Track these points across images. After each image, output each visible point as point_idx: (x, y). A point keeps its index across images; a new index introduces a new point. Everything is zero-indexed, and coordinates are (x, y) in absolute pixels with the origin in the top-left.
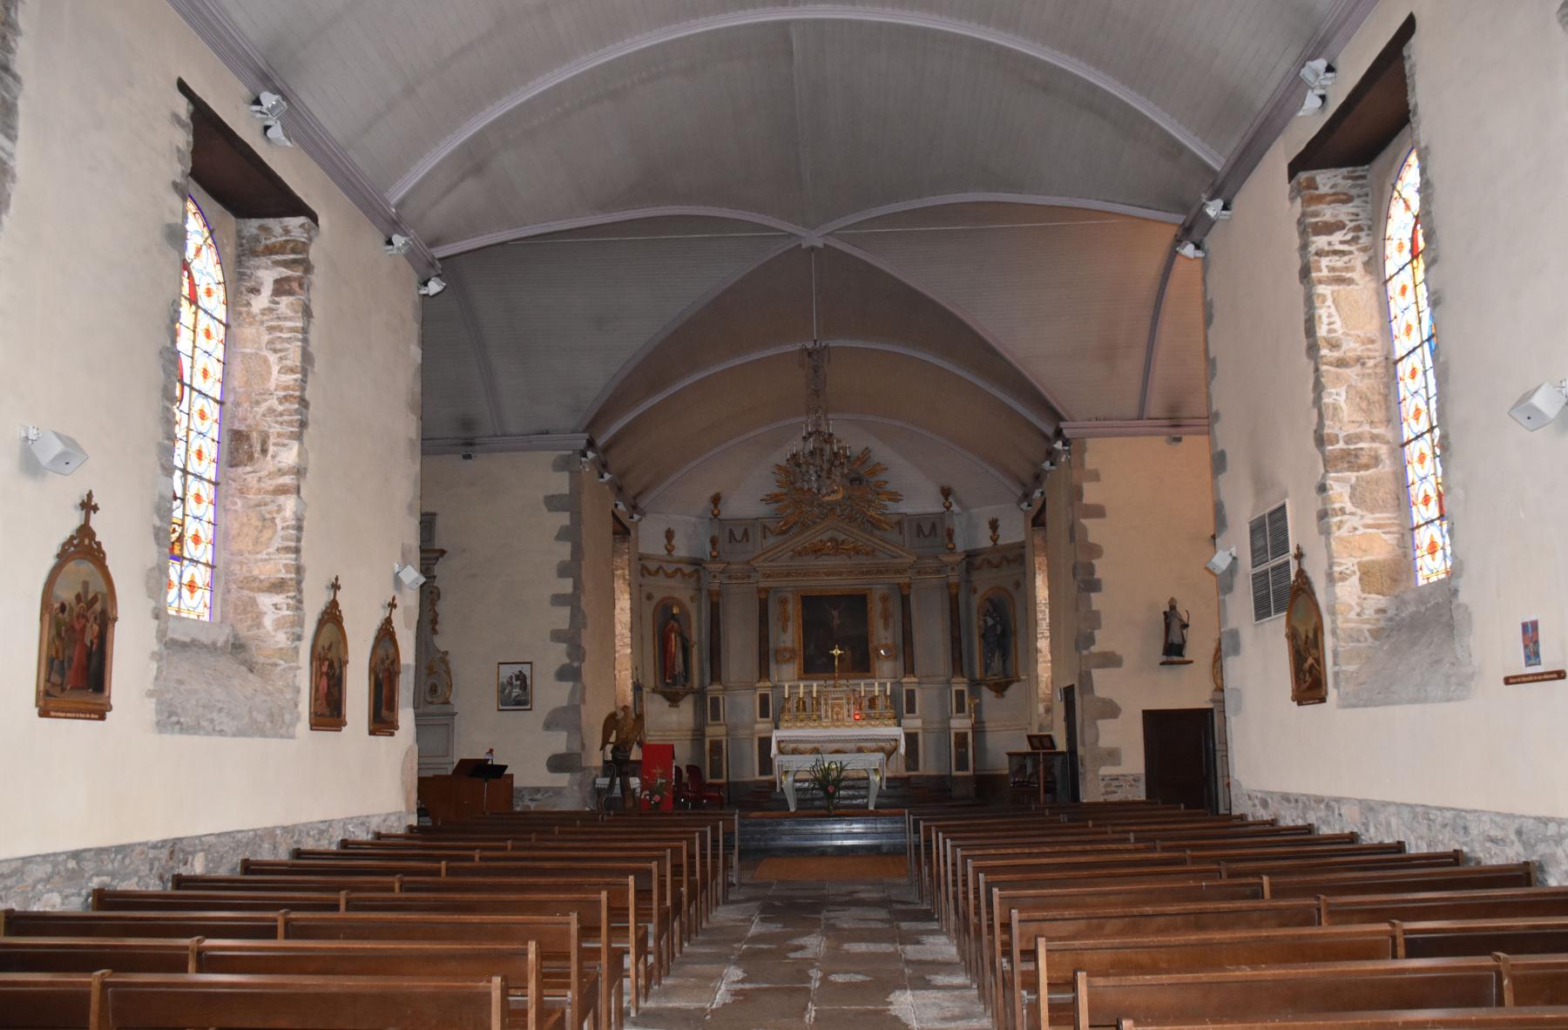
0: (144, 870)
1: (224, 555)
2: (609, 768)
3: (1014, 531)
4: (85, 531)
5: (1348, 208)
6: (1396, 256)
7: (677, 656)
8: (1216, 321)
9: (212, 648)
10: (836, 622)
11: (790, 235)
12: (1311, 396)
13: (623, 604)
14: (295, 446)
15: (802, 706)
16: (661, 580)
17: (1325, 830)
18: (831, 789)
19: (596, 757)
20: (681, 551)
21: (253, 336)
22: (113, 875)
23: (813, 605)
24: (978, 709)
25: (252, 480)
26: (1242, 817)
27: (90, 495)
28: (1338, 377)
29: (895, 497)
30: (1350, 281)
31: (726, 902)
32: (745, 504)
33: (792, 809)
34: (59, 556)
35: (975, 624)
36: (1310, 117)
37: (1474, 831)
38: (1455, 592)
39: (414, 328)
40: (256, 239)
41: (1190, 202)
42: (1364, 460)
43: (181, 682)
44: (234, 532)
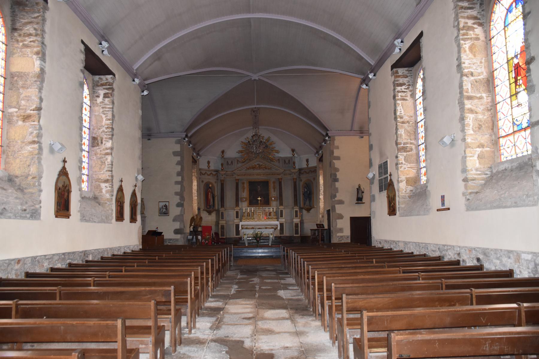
0: (79, 258)
1: (91, 172)
2: (191, 233)
3: (313, 162)
4: (64, 168)
5: (407, 79)
6: (419, 94)
7: (211, 200)
8: (371, 107)
9: (89, 198)
10: (259, 189)
11: (248, 76)
12: (395, 131)
13: (195, 183)
14: (111, 141)
15: (248, 215)
16: (206, 176)
17: (395, 250)
18: (258, 239)
19: (188, 229)
20: (212, 167)
21: (98, 110)
22: (72, 259)
23: (253, 185)
24: (302, 216)
25: (98, 151)
26: (374, 246)
27: (65, 158)
28: (402, 126)
29: (278, 152)
30: (406, 100)
31: (230, 270)
32: (232, 153)
33: (247, 245)
34: (59, 175)
35: (301, 191)
36: (397, 54)
37: (429, 249)
38: (427, 187)
39: (140, 105)
40: (98, 82)
41: (365, 72)
42: (408, 149)
43: (85, 208)
44: (94, 166)
